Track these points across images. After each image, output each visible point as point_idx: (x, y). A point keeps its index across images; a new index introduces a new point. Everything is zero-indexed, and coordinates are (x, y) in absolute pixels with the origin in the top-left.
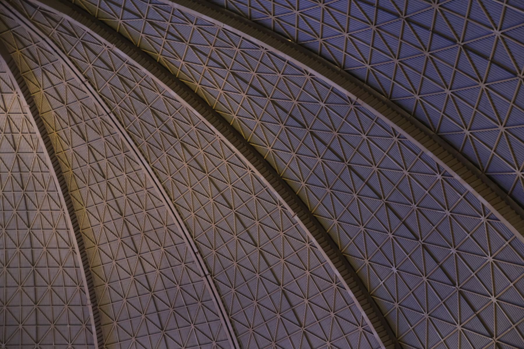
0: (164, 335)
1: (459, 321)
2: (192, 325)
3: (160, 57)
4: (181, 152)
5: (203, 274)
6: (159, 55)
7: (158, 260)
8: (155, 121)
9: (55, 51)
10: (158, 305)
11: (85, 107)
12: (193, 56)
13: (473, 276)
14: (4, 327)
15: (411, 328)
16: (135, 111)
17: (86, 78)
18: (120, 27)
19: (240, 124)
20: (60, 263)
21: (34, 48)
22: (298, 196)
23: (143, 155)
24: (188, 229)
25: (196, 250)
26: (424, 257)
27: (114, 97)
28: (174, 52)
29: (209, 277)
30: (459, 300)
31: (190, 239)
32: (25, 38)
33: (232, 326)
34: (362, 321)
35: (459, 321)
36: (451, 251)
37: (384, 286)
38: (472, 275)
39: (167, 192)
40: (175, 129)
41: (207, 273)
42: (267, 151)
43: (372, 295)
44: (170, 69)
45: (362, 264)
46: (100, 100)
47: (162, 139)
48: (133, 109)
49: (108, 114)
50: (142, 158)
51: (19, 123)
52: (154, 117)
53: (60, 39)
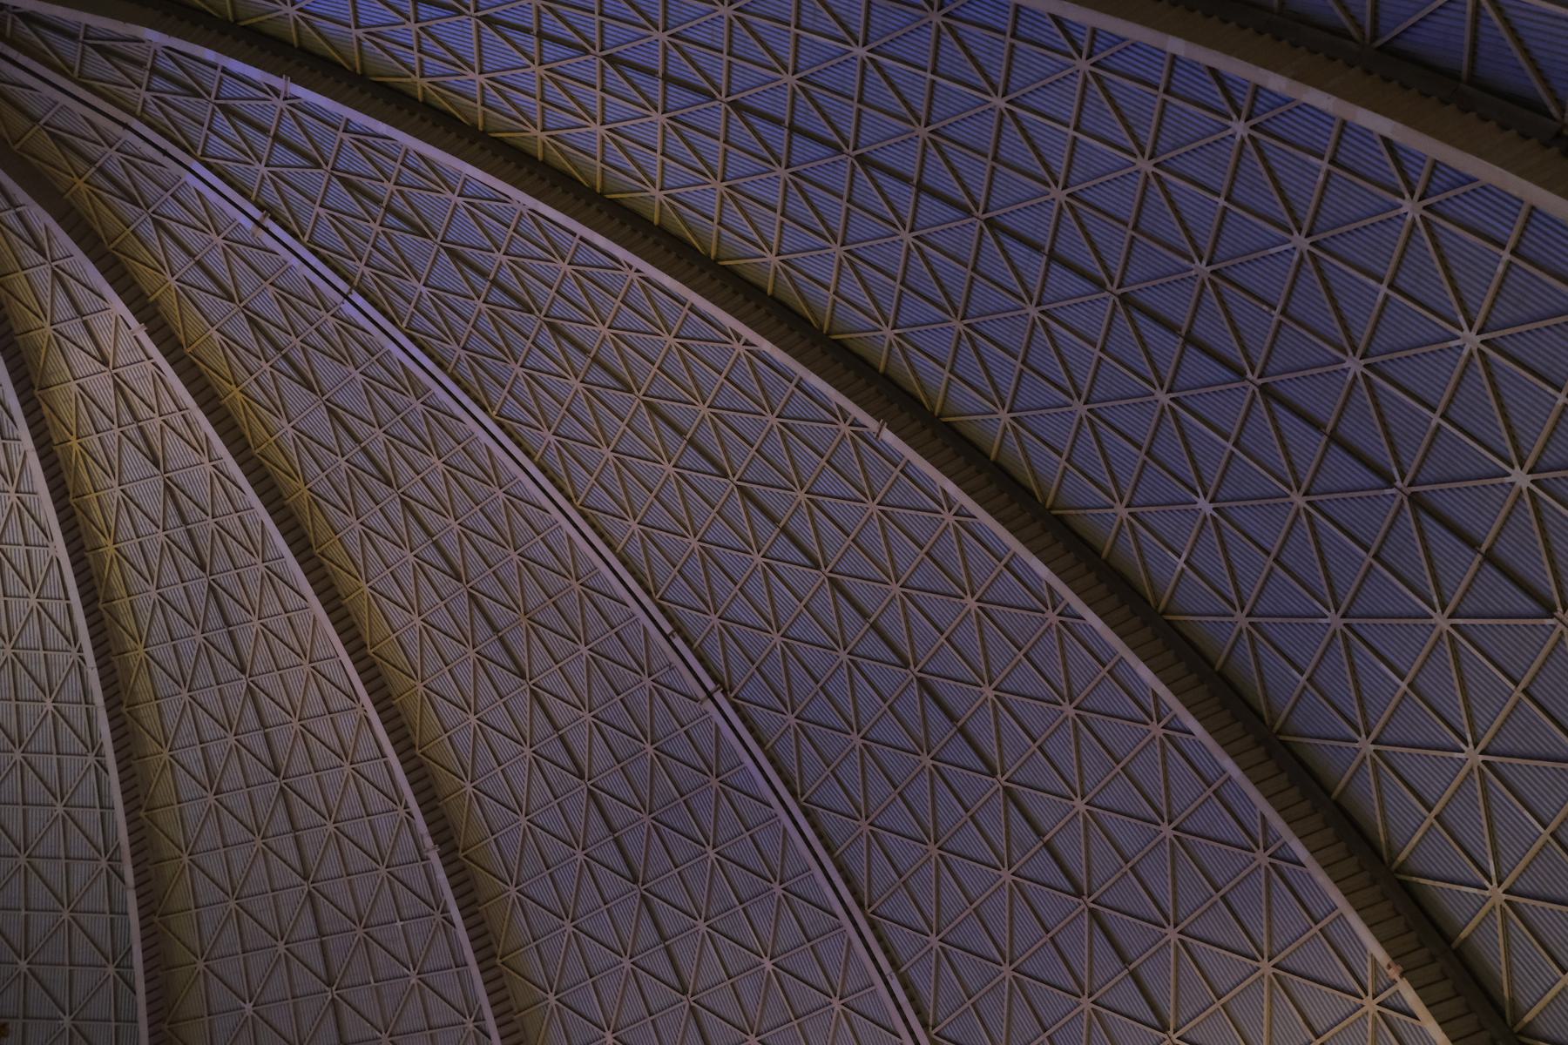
0: (643, 896)
1: (1435, 599)
2: (709, 849)
3: (420, 85)
4: (230, 132)
5: (702, 694)
6: (416, 78)
7: (581, 682)
8: (467, 280)
9: (165, 153)
10: (611, 814)
11: (286, 296)
12: (499, 49)
13: (1439, 427)
14: (241, 956)
15: (1303, 679)
16: (409, 266)
17: (261, 208)
18: (298, 35)
19: (679, 215)
20: (343, 753)
21: (113, 161)
22: (996, 464)
23: (466, 391)
24: (633, 574)
25: (668, 629)
26: (1277, 429)
27: (348, 242)
28: (451, 57)
29: (719, 696)
30: (1420, 529)
31: (645, 599)
32: (84, 138)
33: (814, 826)
34: (1157, 705)
35: (1435, 599)
36: (1346, 371)
37: (1190, 572)
38: (1434, 424)
39: (552, 481)
40: (520, 289)
41: (710, 685)
42: (766, 265)
43: (1164, 612)
44: (458, 110)
45: (1108, 519)
46: (314, 261)
47: (499, 330)
48: (401, 262)
49: (346, 297)
50: (465, 400)
51: (146, 389)
52: (461, 271)
53: (167, 116)
